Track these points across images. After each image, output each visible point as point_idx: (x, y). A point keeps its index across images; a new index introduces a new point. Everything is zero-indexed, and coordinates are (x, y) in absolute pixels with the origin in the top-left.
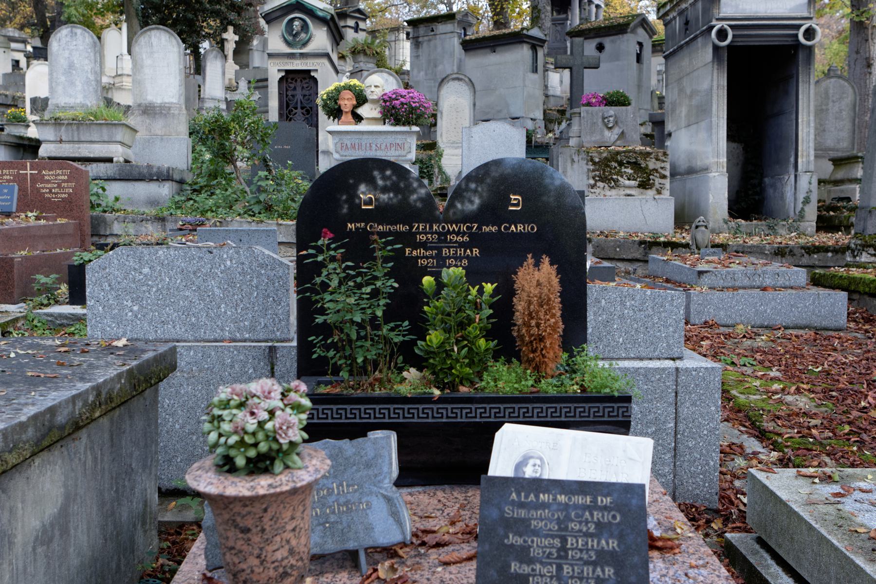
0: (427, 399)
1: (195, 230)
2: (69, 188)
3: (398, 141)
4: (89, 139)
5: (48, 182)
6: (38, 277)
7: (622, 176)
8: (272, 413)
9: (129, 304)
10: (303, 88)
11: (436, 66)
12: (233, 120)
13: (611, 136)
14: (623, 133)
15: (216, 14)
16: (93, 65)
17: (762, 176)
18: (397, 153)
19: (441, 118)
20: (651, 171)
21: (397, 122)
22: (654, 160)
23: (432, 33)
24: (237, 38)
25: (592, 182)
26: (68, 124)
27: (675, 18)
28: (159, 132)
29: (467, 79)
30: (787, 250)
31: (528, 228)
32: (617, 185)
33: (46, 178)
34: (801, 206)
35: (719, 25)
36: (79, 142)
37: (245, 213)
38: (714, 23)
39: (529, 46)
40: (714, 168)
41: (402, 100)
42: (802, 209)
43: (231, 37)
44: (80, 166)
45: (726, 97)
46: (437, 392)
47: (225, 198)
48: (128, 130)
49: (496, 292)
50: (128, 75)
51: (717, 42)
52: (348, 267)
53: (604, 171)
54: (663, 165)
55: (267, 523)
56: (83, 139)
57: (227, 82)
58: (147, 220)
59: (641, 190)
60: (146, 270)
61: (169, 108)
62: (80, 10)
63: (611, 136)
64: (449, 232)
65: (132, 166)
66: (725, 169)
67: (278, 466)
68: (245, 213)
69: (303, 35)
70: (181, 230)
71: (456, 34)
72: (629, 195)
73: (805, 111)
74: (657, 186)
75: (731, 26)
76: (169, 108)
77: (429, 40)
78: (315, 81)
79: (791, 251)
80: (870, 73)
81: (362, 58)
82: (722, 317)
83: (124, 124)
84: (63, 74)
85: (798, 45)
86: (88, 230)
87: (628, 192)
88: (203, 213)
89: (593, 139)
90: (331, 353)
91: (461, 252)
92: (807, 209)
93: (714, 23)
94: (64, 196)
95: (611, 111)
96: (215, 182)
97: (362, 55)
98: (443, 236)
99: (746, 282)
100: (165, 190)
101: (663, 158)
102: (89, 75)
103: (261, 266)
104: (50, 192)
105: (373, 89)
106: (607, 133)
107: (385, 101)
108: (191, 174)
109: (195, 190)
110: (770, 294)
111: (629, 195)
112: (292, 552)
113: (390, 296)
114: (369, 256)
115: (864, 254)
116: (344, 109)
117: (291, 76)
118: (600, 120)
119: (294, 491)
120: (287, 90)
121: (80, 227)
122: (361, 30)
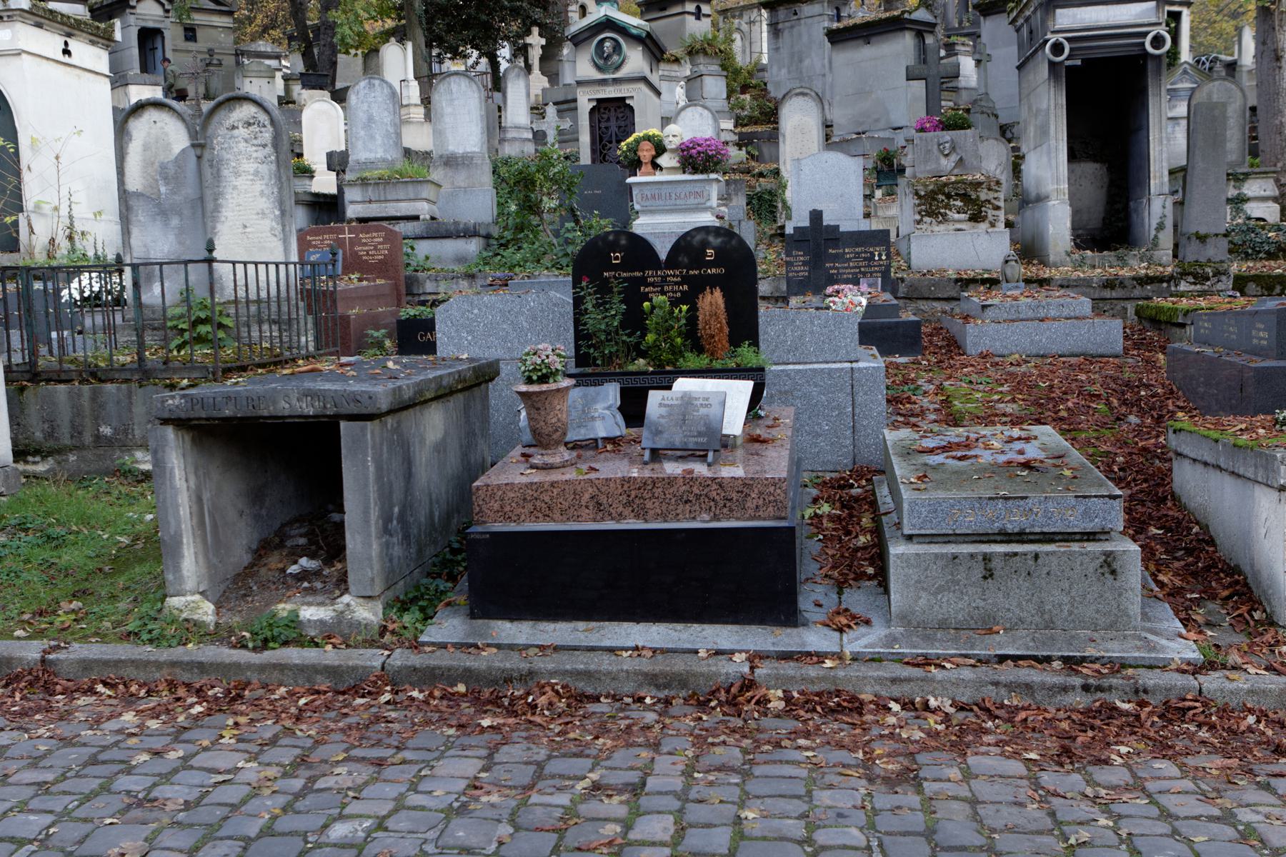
0: (645, 373)
1: (507, 285)
2: (384, 250)
3: (696, 190)
4: (395, 198)
5: (365, 244)
6: (370, 332)
7: (950, 210)
8: (548, 357)
9: (465, 335)
10: (617, 118)
11: (801, 61)
12: (538, 171)
13: (947, 164)
14: (961, 159)
15: (515, 12)
16: (392, 117)
17: (1128, 200)
18: (696, 201)
19: (784, 142)
20: (983, 202)
21: (695, 170)
22: (985, 190)
23: (795, 17)
24: (543, 41)
25: (918, 217)
26: (376, 184)
27: (1022, 25)
28: (462, 184)
29: (813, 94)
30: (1117, 282)
31: (719, 271)
32: (945, 219)
33: (364, 241)
34: (1153, 233)
35: (1053, 38)
36: (386, 201)
37: (553, 266)
38: (1049, 36)
39: (914, 33)
40: (1054, 196)
41: (699, 148)
42: (1156, 236)
43: (536, 40)
44: (391, 227)
45: (1065, 116)
46: (651, 369)
47: (533, 252)
48: (433, 186)
49: (688, 311)
50: (416, 105)
51: (1051, 57)
52: (597, 299)
53: (931, 205)
54: (996, 195)
55: (547, 406)
56: (389, 198)
57: (533, 98)
58: (458, 278)
59: (973, 224)
60: (476, 311)
61: (472, 158)
62: (355, 29)
63: (947, 164)
64: (668, 276)
65: (438, 223)
66: (1067, 196)
67: (551, 380)
68: (553, 266)
69: (615, 58)
70: (491, 285)
71: (826, 17)
72: (959, 230)
73: (1157, 127)
74: (990, 218)
75: (1067, 39)
76: (472, 158)
77: (792, 27)
78: (631, 109)
79: (1121, 283)
80: (1280, 68)
81: (701, 59)
82: (997, 347)
83: (428, 181)
84: (363, 128)
85: (1146, 55)
86: (404, 292)
87: (959, 226)
88: (511, 268)
89: (928, 168)
90: (592, 351)
91: (676, 288)
92: (1161, 235)
93: (1049, 36)
94: (380, 257)
95: (947, 136)
96: (521, 235)
97: (701, 55)
98: (664, 278)
99: (1030, 314)
100: (472, 247)
101: (996, 188)
102: (389, 128)
103: (555, 305)
104: (368, 254)
105: (671, 138)
106: (944, 161)
107: (683, 151)
108: (497, 228)
109: (501, 245)
110: (1044, 325)
111: (959, 230)
112: (559, 420)
113: (623, 314)
114: (610, 291)
115: (1183, 283)
116: (644, 161)
117: (604, 105)
118: (936, 147)
119: (558, 390)
120: (600, 122)
121: (396, 287)
122: (704, 15)
